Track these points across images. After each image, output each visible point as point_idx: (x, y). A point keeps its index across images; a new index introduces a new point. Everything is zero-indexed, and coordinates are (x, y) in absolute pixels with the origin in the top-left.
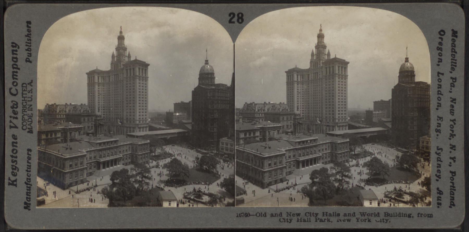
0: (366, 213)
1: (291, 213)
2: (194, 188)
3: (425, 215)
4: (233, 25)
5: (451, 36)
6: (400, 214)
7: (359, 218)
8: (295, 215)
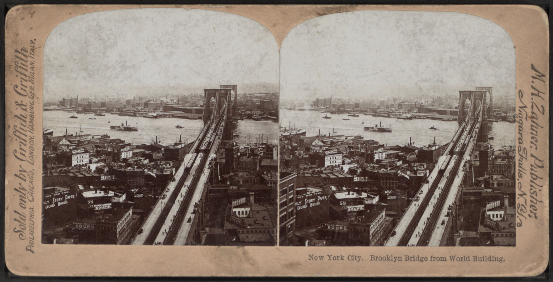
0: (331, 255)
1: (313, 255)
2: (444, 220)
3: (438, 259)
4: (210, 249)
7: (331, 255)
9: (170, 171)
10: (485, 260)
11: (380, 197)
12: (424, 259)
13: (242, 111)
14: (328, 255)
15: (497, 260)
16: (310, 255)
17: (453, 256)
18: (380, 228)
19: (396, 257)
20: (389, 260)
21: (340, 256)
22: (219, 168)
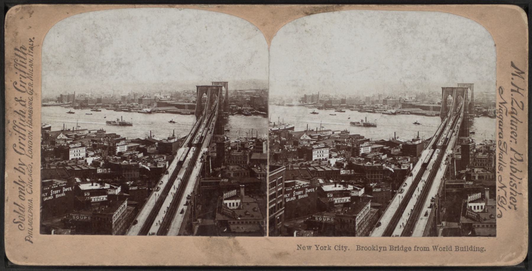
0: (319, 245)
1: (301, 245)
3: (421, 249)
5: (49, 235)
6: (403, 248)
7: (319, 245)
8: (305, 247)
9: (164, 164)
10: (466, 250)
11: (365, 190)
12: (407, 249)
13: (233, 107)
14: (316, 246)
15: (478, 250)
16: (298, 245)
17: (435, 246)
18: (366, 219)
19: (381, 247)
20: (375, 250)
21: (327, 246)
22: (211, 162)
